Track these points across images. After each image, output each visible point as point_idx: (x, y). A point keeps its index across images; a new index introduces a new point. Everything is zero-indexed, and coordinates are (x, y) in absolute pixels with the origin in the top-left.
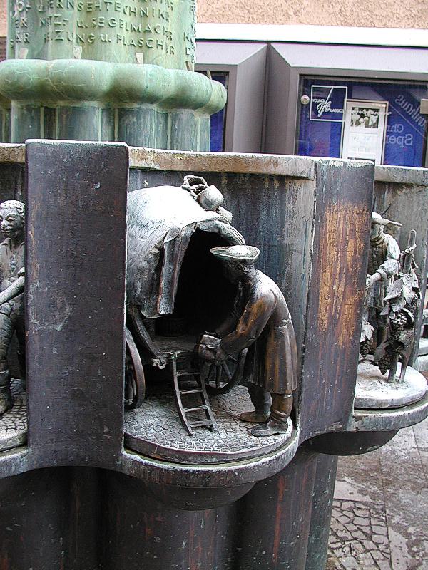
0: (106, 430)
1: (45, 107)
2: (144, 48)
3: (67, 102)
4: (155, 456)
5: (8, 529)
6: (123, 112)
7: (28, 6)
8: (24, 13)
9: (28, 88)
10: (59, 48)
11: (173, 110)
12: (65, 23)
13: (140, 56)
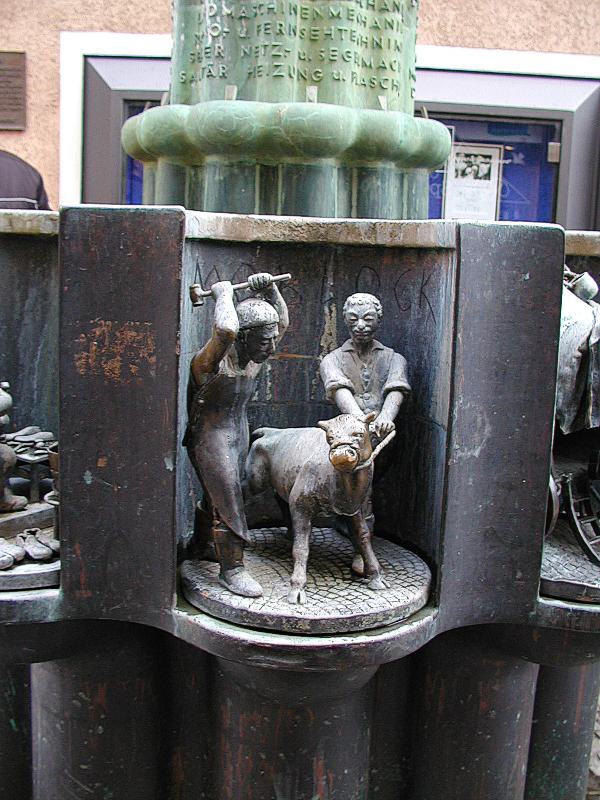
0: (519, 575)
1: (262, 165)
2: (378, 89)
3: (298, 158)
4: (582, 599)
5: (327, 723)
6: (364, 173)
7: (226, 30)
8: (221, 39)
9: (249, 139)
10: (278, 86)
11: (411, 170)
12: (287, 54)
13: (312, 91)
